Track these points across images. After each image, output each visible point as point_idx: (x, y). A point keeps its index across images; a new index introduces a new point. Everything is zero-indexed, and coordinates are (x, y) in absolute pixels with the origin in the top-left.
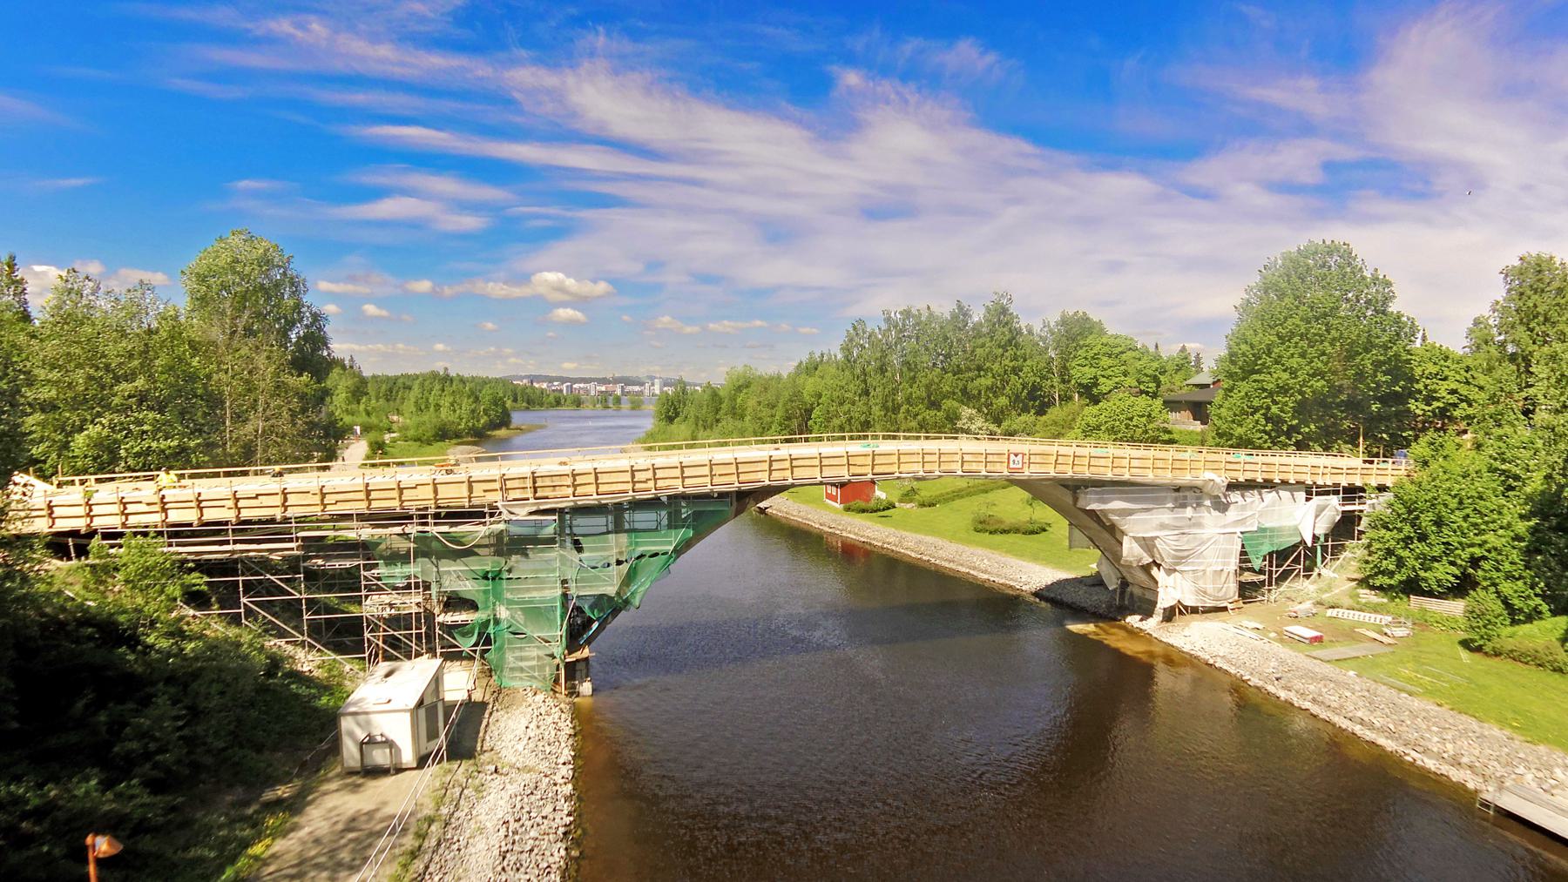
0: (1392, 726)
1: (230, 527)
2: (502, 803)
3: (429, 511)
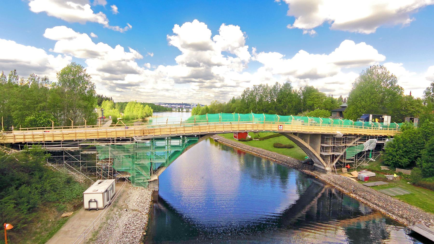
0: (384, 206)
1: (61, 142)
2: (126, 219)
3: (115, 139)
